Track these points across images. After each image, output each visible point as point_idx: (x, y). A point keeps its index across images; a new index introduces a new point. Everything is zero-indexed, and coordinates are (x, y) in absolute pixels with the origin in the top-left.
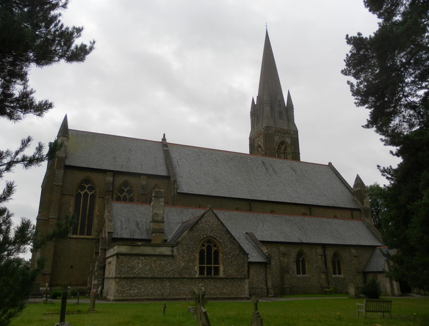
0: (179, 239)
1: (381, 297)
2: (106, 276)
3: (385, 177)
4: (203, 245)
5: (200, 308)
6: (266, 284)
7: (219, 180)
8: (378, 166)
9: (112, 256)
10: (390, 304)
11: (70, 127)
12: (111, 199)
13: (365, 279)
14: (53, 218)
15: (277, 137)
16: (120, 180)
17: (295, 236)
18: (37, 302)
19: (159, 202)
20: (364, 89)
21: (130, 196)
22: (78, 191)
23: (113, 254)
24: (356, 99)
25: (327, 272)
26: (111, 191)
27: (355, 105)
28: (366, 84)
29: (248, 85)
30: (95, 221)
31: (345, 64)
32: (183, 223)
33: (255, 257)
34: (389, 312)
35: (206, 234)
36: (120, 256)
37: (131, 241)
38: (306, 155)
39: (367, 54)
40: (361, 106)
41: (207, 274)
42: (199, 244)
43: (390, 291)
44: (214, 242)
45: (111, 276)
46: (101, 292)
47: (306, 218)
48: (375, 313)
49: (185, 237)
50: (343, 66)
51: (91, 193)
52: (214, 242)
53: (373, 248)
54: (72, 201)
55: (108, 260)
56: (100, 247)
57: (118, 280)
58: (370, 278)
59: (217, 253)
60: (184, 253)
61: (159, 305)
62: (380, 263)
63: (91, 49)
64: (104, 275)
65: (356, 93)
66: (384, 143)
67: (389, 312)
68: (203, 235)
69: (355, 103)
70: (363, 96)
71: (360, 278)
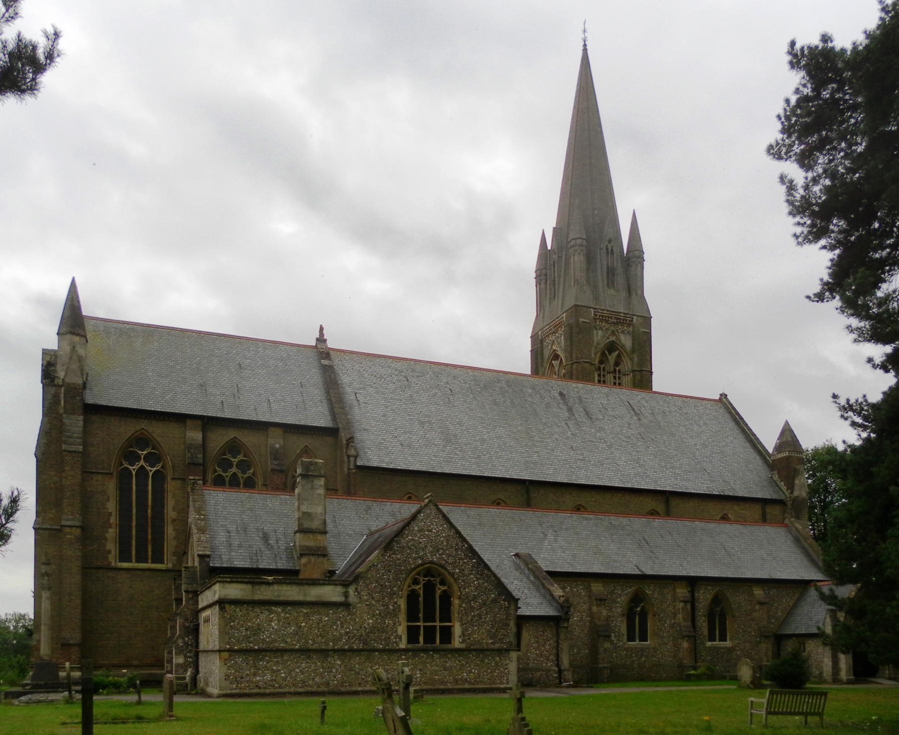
0: (360, 570)
1: (808, 685)
2: (202, 646)
3: (848, 422)
4: (415, 582)
5: (393, 708)
6: (558, 660)
7: (455, 436)
8: (835, 396)
9: (209, 606)
10: (823, 698)
11: (85, 311)
12: (201, 482)
13: (779, 649)
14: (71, 527)
15: (600, 333)
16: (219, 439)
17: (628, 562)
18: (52, 701)
19: (312, 488)
20: (820, 198)
21: (246, 476)
22: (122, 464)
23: (211, 601)
24: (799, 224)
25: (695, 637)
26: (200, 465)
27: (793, 241)
28: (828, 182)
29: (526, 194)
30: (170, 531)
31: (779, 126)
32: (372, 534)
33: (533, 604)
34: (820, 715)
35: (421, 558)
36: (227, 606)
37: (252, 575)
38: (665, 377)
39: (840, 99)
40: (810, 242)
41: (424, 643)
42: (405, 579)
43: (830, 674)
44: (439, 575)
45: (210, 647)
46: (194, 679)
47: (657, 522)
48: (789, 718)
50: (773, 133)
52: (439, 575)
53: (803, 585)
54: (111, 487)
55: (204, 614)
56: (183, 587)
57: (225, 655)
58: (789, 647)
59: (446, 598)
60: (373, 598)
61: (313, 705)
62: (815, 616)
63: (50, 56)
65: (801, 207)
66: (854, 336)
67: (820, 715)
68: (415, 559)
69: (796, 236)
70: (817, 216)
71: (766, 647)
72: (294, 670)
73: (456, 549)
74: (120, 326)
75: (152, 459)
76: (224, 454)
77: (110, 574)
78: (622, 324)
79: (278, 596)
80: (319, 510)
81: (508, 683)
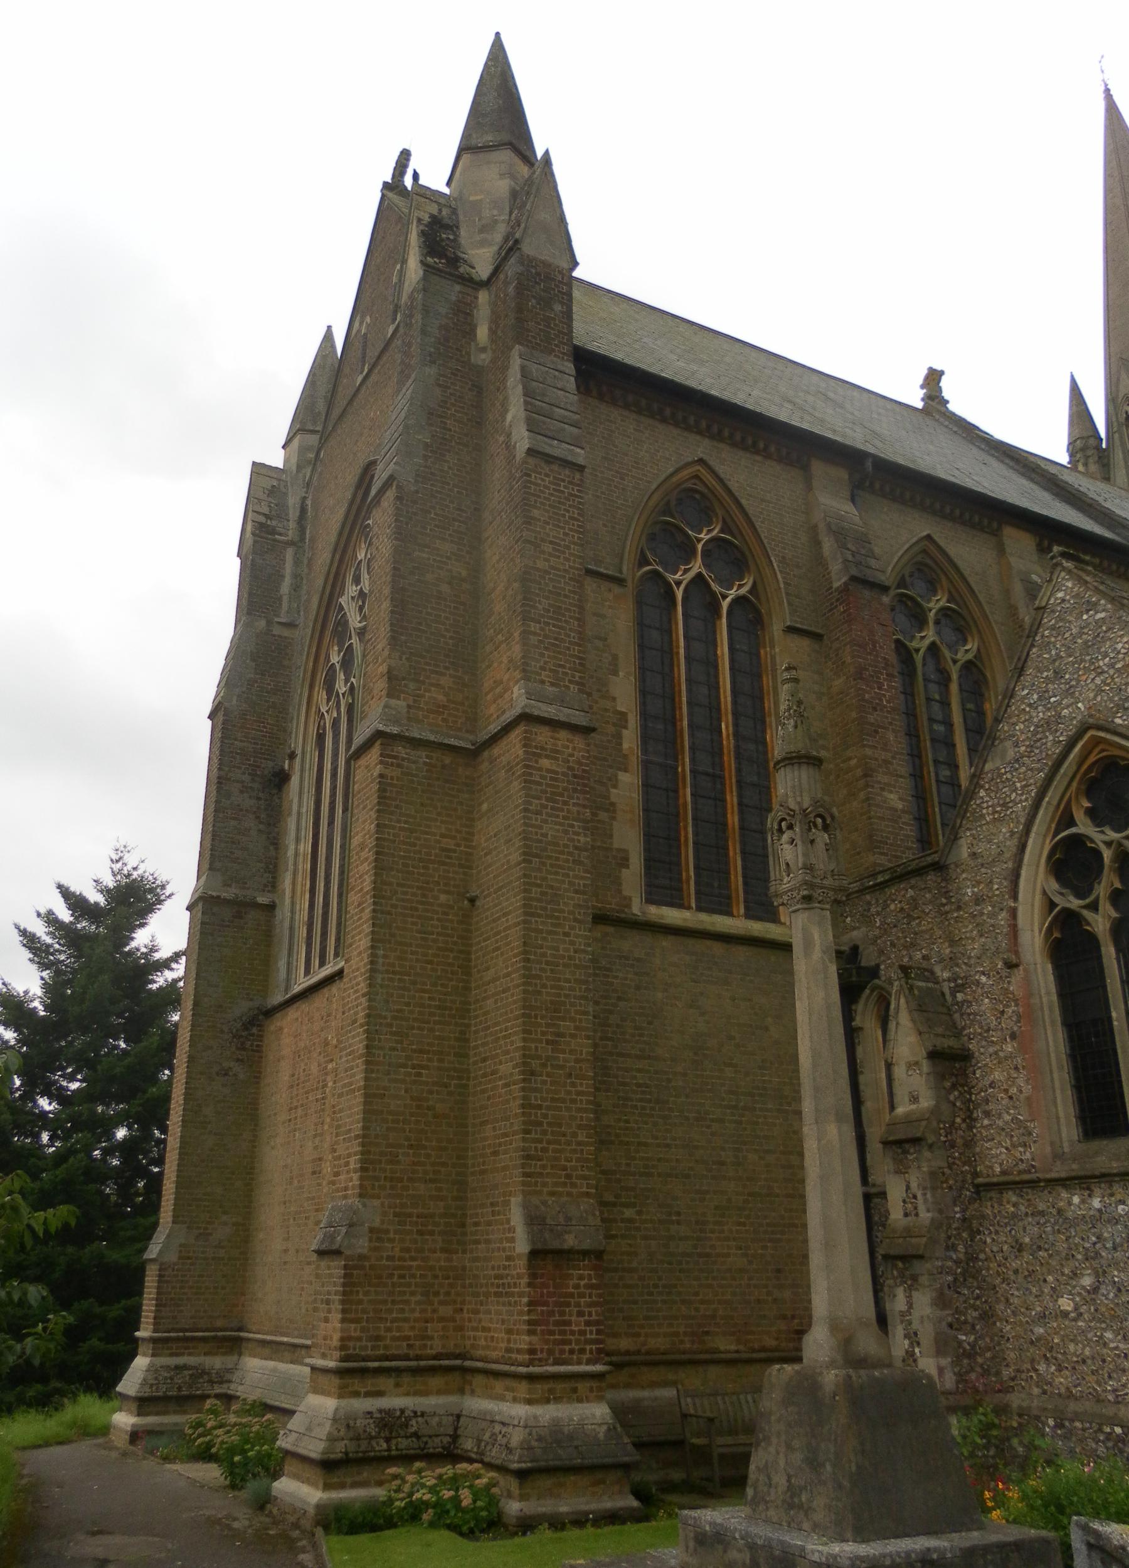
51: (732, 593)
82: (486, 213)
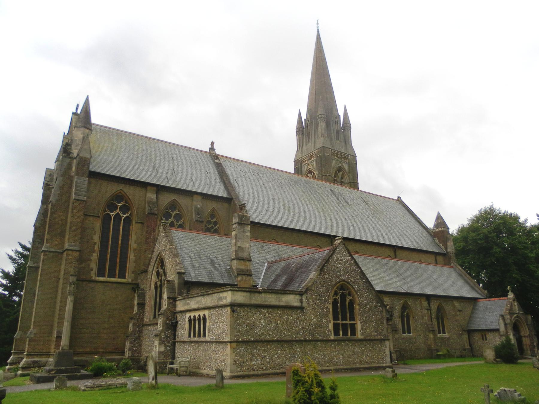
2: (178, 339)
4: (336, 293)
14: (72, 250)
16: (166, 199)
19: (244, 232)
22: (106, 211)
29: (297, 101)
42: (331, 291)
49: (315, 282)
51: (125, 216)
54: (98, 225)
57: (234, 345)
59: (352, 303)
60: (315, 304)
64: (175, 339)
68: (336, 278)
72: (274, 355)
73: (355, 273)
74: (102, 128)
75: (125, 209)
76: (167, 209)
77: (90, 285)
78: (344, 158)
79: (265, 301)
80: (247, 245)
81: (386, 363)
82: (78, 142)
